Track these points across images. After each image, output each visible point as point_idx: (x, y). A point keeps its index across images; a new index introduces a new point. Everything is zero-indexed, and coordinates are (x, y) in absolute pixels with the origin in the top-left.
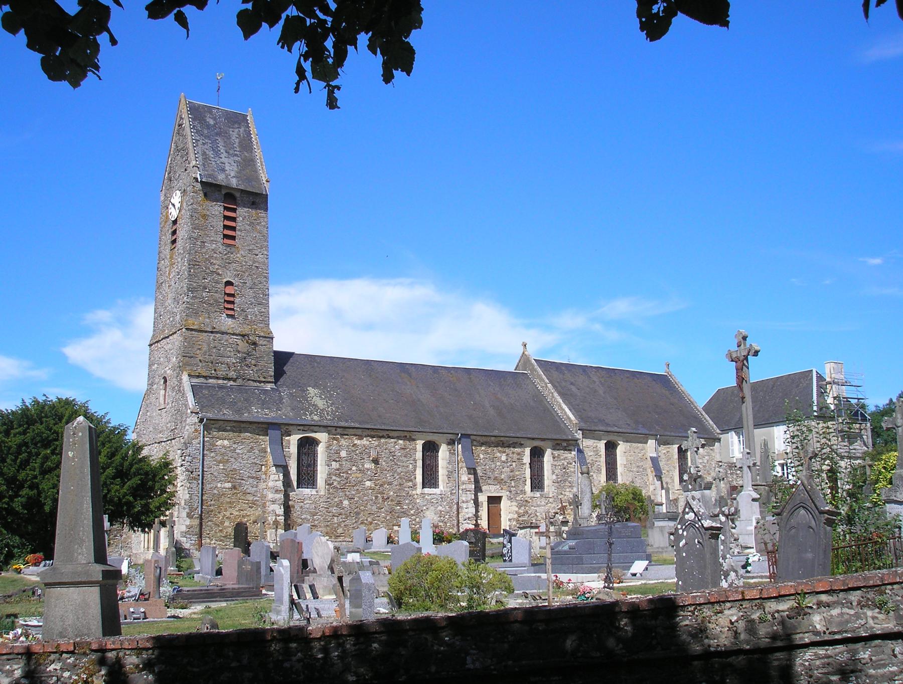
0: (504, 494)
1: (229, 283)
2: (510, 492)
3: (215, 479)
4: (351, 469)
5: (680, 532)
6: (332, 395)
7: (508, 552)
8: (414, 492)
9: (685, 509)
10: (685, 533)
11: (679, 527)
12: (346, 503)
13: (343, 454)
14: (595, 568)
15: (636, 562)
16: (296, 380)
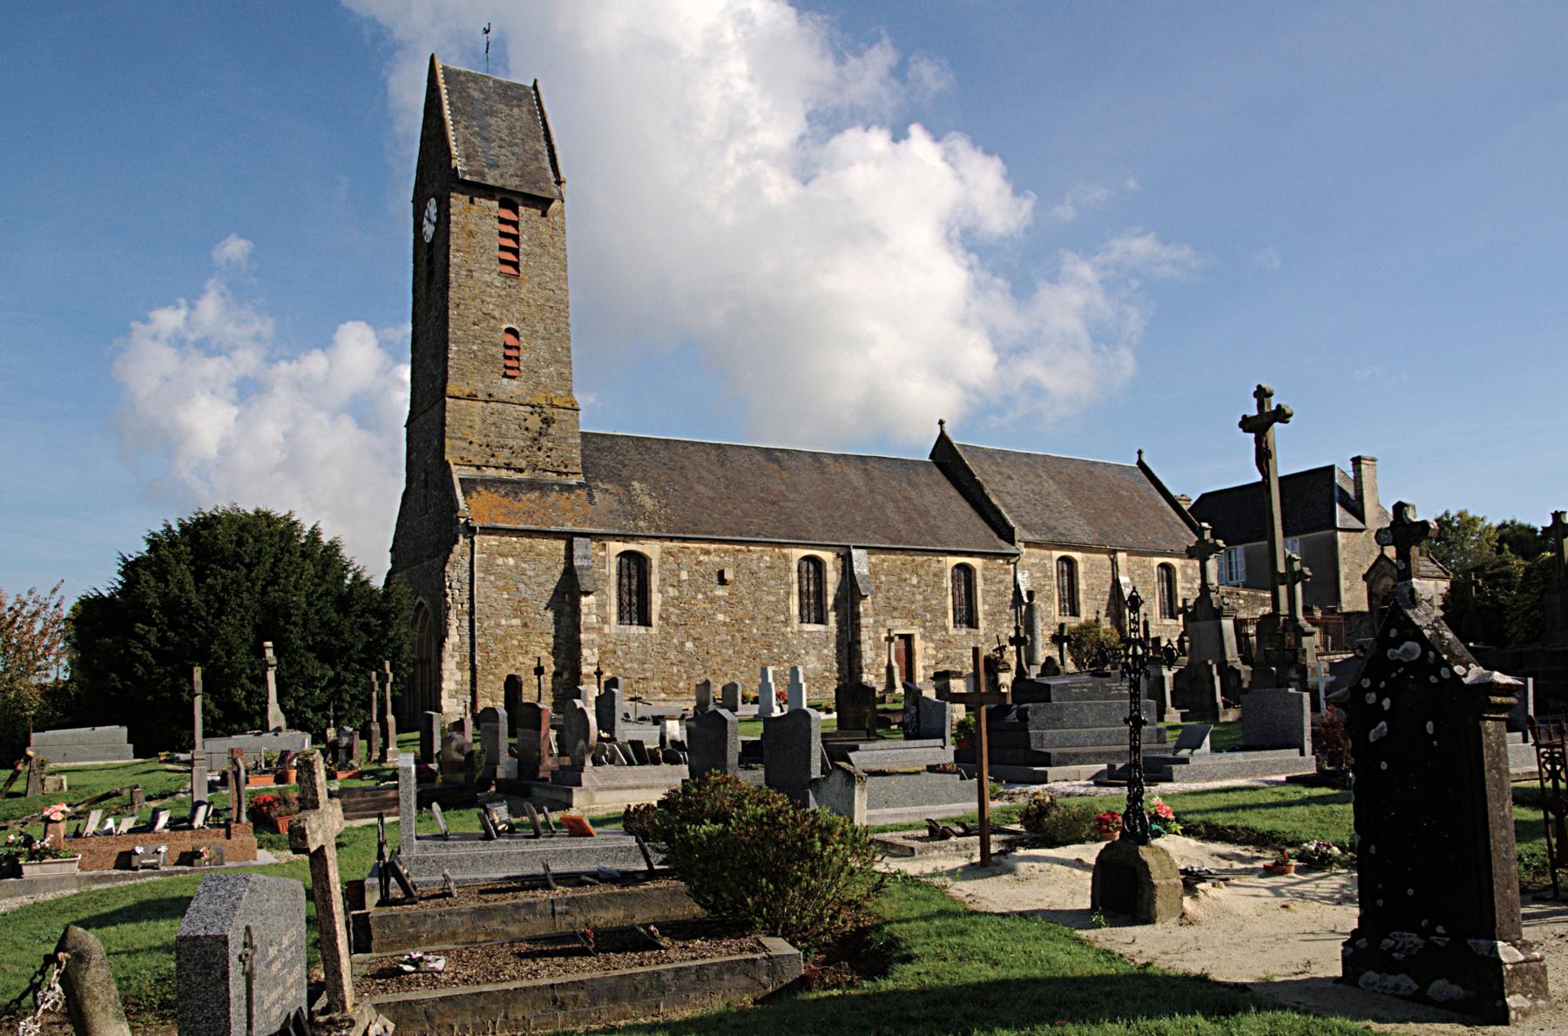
0: (916, 632)
1: (510, 331)
2: (925, 628)
3: (496, 613)
4: (695, 598)
5: (1372, 698)
6: (666, 494)
7: (912, 721)
8: (789, 629)
9: (1385, 632)
10: (1386, 703)
11: (1366, 683)
12: (689, 645)
13: (684, 575)
14: (1066, 755)
15: (363, 324)
16: (615, 471)
